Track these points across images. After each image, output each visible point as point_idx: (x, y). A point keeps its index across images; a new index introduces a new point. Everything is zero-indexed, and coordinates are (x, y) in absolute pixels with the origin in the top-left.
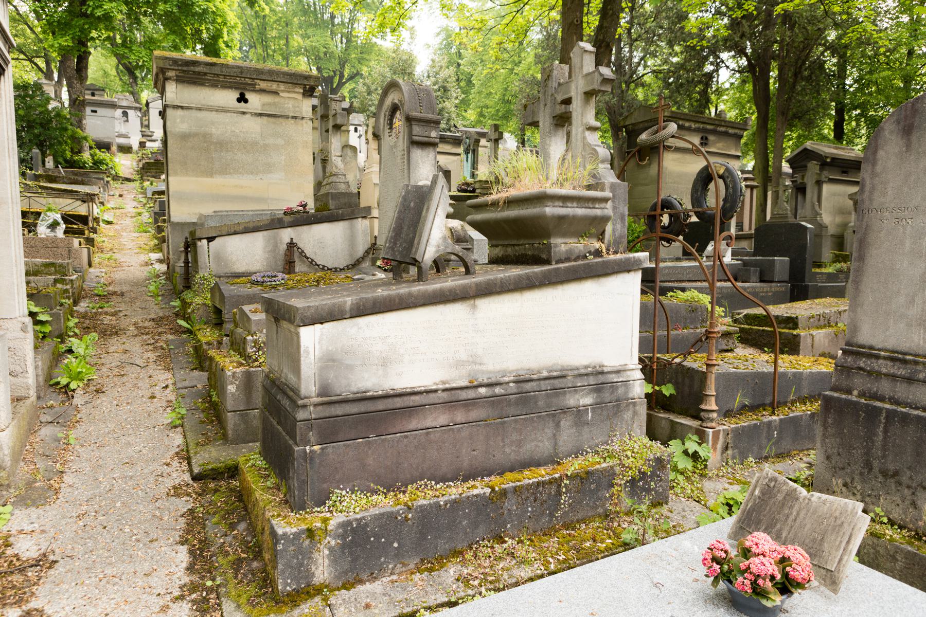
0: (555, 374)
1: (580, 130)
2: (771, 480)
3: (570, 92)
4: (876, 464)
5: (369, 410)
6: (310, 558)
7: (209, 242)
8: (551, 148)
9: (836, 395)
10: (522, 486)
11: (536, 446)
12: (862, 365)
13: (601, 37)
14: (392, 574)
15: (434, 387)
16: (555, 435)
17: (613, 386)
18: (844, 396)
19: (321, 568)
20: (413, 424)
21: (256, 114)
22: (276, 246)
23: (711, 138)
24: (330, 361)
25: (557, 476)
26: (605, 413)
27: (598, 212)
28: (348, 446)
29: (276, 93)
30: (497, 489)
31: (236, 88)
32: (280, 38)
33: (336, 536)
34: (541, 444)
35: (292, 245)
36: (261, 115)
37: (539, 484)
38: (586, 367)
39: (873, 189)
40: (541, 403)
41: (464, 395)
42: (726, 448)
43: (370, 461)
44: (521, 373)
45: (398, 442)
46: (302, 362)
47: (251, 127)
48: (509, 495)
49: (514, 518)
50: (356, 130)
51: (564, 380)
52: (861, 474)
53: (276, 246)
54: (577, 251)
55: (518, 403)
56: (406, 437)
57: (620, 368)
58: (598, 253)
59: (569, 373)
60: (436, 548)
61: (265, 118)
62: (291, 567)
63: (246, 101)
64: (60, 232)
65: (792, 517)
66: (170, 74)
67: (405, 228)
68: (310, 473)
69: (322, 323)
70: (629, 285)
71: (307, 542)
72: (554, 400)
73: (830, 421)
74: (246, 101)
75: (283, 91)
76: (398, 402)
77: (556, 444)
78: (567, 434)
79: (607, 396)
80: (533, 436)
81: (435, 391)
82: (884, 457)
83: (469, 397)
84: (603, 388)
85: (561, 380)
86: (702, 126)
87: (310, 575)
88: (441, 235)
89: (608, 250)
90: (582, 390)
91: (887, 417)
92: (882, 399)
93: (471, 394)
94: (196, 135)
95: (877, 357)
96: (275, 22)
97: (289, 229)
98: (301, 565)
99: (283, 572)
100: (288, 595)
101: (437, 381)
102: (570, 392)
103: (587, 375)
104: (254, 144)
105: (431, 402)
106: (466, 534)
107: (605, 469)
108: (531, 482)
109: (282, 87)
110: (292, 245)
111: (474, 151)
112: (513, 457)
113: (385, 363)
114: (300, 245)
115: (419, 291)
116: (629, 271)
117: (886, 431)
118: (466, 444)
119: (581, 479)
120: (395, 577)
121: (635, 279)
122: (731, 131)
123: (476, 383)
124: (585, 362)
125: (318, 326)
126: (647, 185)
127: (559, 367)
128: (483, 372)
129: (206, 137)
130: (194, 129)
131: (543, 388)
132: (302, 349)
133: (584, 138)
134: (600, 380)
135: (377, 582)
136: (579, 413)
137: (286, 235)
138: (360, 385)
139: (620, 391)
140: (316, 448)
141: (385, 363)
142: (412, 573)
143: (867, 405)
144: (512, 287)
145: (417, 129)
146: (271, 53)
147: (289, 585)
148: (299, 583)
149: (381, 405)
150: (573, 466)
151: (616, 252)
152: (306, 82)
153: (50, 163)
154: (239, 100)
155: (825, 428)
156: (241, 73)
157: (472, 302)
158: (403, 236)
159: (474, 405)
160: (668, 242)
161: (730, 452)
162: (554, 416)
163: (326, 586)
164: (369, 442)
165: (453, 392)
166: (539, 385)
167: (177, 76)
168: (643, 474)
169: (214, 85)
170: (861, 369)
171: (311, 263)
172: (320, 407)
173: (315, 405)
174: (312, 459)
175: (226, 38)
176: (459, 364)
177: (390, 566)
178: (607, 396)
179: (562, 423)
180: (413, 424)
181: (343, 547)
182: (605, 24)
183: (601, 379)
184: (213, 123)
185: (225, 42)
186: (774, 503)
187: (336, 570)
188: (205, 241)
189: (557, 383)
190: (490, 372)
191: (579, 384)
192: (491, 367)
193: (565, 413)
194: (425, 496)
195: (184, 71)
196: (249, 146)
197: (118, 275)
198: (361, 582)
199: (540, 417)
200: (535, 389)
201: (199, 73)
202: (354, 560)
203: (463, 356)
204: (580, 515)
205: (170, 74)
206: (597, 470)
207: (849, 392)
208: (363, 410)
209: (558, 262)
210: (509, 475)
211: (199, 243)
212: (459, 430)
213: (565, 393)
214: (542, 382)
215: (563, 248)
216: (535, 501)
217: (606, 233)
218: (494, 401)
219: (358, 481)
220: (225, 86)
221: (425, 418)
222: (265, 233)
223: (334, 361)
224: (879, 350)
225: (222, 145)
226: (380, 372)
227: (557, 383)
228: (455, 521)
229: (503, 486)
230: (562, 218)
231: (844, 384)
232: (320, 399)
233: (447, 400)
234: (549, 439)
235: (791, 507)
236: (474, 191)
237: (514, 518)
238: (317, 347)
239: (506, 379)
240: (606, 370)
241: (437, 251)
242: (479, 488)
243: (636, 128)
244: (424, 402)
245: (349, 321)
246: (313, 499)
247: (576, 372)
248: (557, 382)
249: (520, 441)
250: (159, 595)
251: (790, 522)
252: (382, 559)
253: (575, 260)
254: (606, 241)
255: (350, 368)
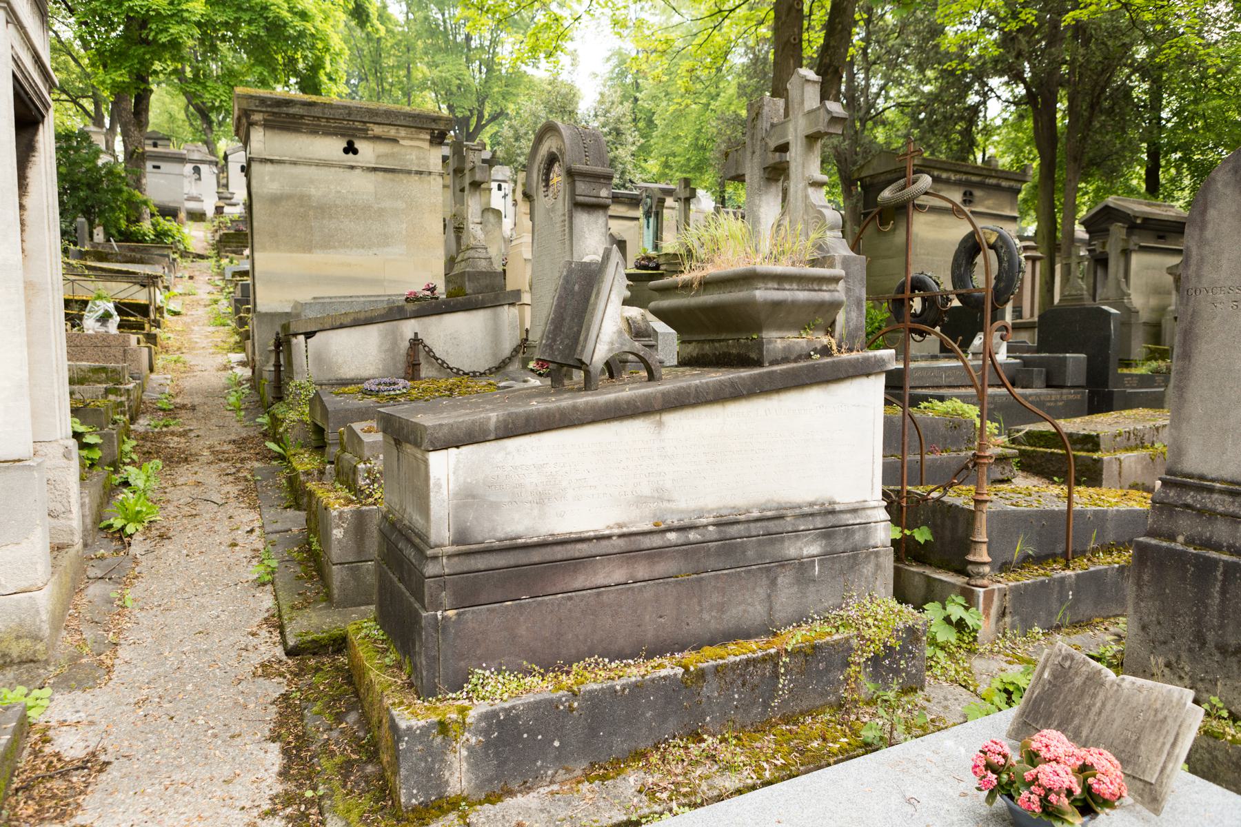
0: (769, 514)
1: (801, 186)
2: (1065, 658)
3: (787, 136)
4: (1210, 636)
5: (520, 563)
6: (443, 760)
7: (307, 338)
8: (762, 210)
9: (1154, 542)
10: (726, 666)
11: (745, 611)
12: (1190, 501)
13: (827, 60)
14: (552, 782)
15: (607, 532)
16: (769, 596)
17: (848, 529)
18: (1164, 544)
19: (457, 774)
20: (580, 581)
21: (368, 168)
22: (395, 343)
23: (978, 193)
24: (468, 497)
25: (773, 651)
26: (837, 566)
27: (826, 296)
28: (494, 610)
29: (394, 141)
30: (692, 669)
31: (343, 135)
32: (399, 67)
33: (478, 732)
34: (751, 609)
35: (416, 342)
36: (375, 169)
37: (748, 662)
38: (811, 505)
39: (1202, 260)
40: (750, 553)
41: (647, 542)
42: (1003, 614)
43: (522, 631)
44: (723, 512)
45: (559, 605)
46: (432, 499)
47: (362, 186)
48: (709, 678)
49: (715, 708)
50: (500, 188)
51: (782, 522)
52: (1190, 650)
53: (395, 343)
54: (797, 348)
55: (719, 552)
56: (570, 598)
57: (857, 506)
58: (826, 351)
59: (789, 512)
60: (611, 748)
61: (381, 174)
62: (417, 772)
63: (355, 152)
64: (113, 327)
65: (1095, 709)
66: (257, 117)
67: (568, 319)
68: (442, 647)
69: (458, 447)
70: (865, 400)
71: (439, 739)
72: (768, 549)
73: (1146, 577)
74: (355, 152)
75: (403, 138)
76: (560, 552)
77: (771, 609)
78: (786, 595)
79: (840, 543)
80: (740, 598)
81: (609, 537)
82: (1222, 627)
83: (654, 545)
84: (834, 532)
85: (777, 522)
86: (964, 177)
87: (442, 784)
88: (615, 329)
89: (839, 346)
90: (806, 536)
91: (1225, 573)
92: (1218, 548)
93: (656, 541)
94: (289, 197)
95: (1211, 490)
96: (392, 47)
97: (413, 321)
98: (431, 770)
99: (407, 778)
100: (413, 810)
101: (611, 523)
102: (789, 538)
103: (812, 515)
104: (366, 208)
105: (603, 552)
106: (651, 729)
107: (837, 643)
108: (738, 659)
109: (403, 132)
110: (416, 342)
111: (657, 214)
112: (713, 625)
113: (542, 500)
114: (427, 342)
115: (587, 403)
116: (868, 375)
117: (1223, 592)
118: (650, 609)
119: (806, 655)
120: (555, 787)
121: (877, 385)
122: (1004, 184)
123: (663, 526)
124: (810, 498)
125: (453, 451)
126: (891, 257)
127: (775, 505)
128: (673, 512)
129: (303, 199)
130: (287, 190)
131: (754, 533)
132: (432, 482)
133: (807, 197)
134: (830, 522)
135: (532, 794)
136: (802, 566)
137: (409, 328)
138: (509, 530)
139: (858, 537)
140: (451, 613)
141: (542, 500)
142: (579, 782)
143: (1197, 556)
144: (711, 397)
145: (581, 187)
146: (387, 87)
147: (415, 796)
148: (427, 795)
149: (536, 556)
150: (795, 638)
151: (850, 350)
152: (434, 126)
153: (99, 235)
154: (346, 151)
155: (1139, 586)
156: (349, 114)
157: (658, 417)
158: (565, 330)
159: (660, 555)
160: (921, 335)
161: (1008, 619)
162: (768, 570)
163: (464, 799)
164: (521, 605)
165: (633, 538)
166: (748, 529)
167: (265, 120)
168: (890, 649)
169: (314, 131)
170: (1188, 506)
171: (441, 365)
172: (456, 559)
173: (449, 556)
174: (445, 628)
175: (328, 68)
176: (640, 501)
177: (550, 773)
178: (840, 543)
179: (780, 580)
180: (580, 581)
181: (487, 745)
182: (832, 43)
183: (832, 520)
184: (311, 181)
185: (327, 74)
186: (1070, 690)
187: (477, 778)
188: (302, 338)
189: (772, 526)
190: (682, 512)
191: (802, 528)
192: (683, 505)
193: (783, 566)
194: (595, 678)
195: (274, 114)
196: (361, 211)
197: (188, 383)
198: (511, 793)
199: (749, 571)
200: (743, 534)
201: (294, 116)
202: (502, 764)
203: (646, 491)
204: (805, 705)
205: (257, 117)
206: (827, 643)
207: (1172, 538)
208: (512, 562)
209: (772, 363)
210: (708, 651)
211: (294, 341)
212: (640, 589)
213: (783, 540)
214: (752, 525)
215: (779, 344)
216: (744, 685)
217: (837, 323)
218: (688, 551)
219: (506, 658)
220: (328, 133)
221: (595, 573)
222: (381, 326)
223: (474, 497)
224: (1213, 480)
225: (324, 210)
226: (536, 512)
227: (772, 526)
228: (636, 711)
229: (700, 665)
230: (777, 305)
231: (1165, 526)
232: (455, 549)
233: (624, 549)
234: (761, 602)
235: (1094, 696)
236: (657, 267)
237: (715, 708)
238: (452, 478)
239: (704, 521)
240: (837, 508)
241: (610, 350)
242: (668, 668)
243: (876, 181)
244: (594, 552)
245: (493, 443)
246: (446, 681)
247: (798, 511)
248: (773, 524)
249: (723, 604)
250: (243, 808)
251: (1092, 715)
252: (539, 763)
253: (795, 361)
254: (837, 335)
255: (495, 506)
